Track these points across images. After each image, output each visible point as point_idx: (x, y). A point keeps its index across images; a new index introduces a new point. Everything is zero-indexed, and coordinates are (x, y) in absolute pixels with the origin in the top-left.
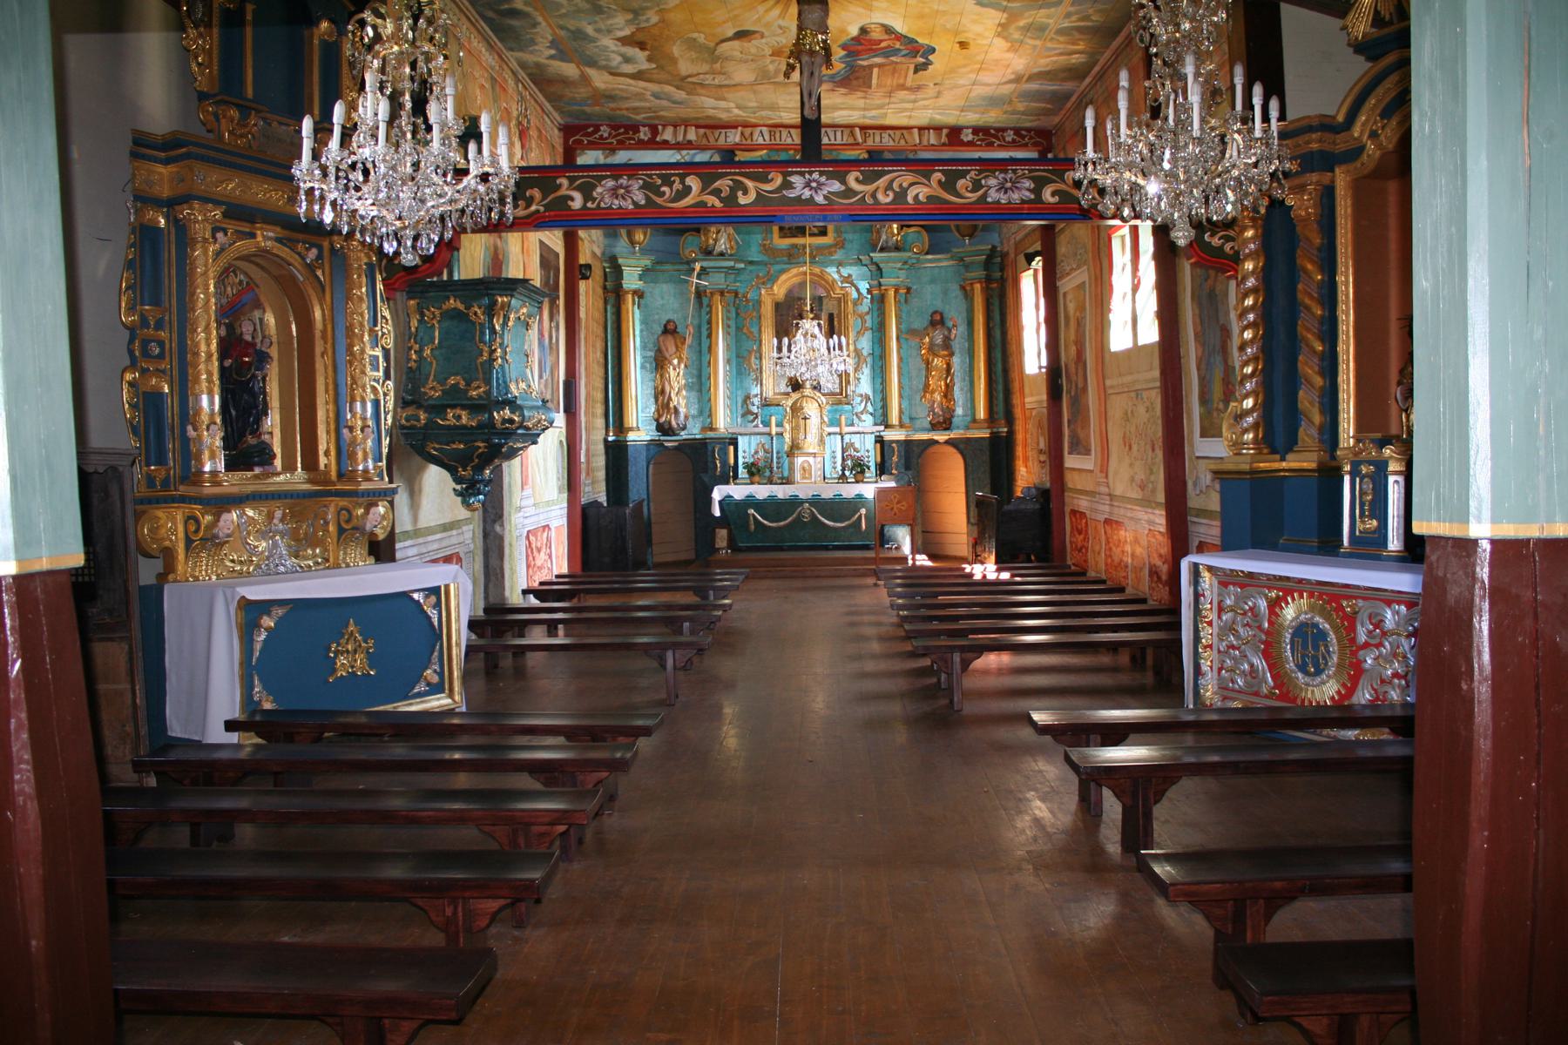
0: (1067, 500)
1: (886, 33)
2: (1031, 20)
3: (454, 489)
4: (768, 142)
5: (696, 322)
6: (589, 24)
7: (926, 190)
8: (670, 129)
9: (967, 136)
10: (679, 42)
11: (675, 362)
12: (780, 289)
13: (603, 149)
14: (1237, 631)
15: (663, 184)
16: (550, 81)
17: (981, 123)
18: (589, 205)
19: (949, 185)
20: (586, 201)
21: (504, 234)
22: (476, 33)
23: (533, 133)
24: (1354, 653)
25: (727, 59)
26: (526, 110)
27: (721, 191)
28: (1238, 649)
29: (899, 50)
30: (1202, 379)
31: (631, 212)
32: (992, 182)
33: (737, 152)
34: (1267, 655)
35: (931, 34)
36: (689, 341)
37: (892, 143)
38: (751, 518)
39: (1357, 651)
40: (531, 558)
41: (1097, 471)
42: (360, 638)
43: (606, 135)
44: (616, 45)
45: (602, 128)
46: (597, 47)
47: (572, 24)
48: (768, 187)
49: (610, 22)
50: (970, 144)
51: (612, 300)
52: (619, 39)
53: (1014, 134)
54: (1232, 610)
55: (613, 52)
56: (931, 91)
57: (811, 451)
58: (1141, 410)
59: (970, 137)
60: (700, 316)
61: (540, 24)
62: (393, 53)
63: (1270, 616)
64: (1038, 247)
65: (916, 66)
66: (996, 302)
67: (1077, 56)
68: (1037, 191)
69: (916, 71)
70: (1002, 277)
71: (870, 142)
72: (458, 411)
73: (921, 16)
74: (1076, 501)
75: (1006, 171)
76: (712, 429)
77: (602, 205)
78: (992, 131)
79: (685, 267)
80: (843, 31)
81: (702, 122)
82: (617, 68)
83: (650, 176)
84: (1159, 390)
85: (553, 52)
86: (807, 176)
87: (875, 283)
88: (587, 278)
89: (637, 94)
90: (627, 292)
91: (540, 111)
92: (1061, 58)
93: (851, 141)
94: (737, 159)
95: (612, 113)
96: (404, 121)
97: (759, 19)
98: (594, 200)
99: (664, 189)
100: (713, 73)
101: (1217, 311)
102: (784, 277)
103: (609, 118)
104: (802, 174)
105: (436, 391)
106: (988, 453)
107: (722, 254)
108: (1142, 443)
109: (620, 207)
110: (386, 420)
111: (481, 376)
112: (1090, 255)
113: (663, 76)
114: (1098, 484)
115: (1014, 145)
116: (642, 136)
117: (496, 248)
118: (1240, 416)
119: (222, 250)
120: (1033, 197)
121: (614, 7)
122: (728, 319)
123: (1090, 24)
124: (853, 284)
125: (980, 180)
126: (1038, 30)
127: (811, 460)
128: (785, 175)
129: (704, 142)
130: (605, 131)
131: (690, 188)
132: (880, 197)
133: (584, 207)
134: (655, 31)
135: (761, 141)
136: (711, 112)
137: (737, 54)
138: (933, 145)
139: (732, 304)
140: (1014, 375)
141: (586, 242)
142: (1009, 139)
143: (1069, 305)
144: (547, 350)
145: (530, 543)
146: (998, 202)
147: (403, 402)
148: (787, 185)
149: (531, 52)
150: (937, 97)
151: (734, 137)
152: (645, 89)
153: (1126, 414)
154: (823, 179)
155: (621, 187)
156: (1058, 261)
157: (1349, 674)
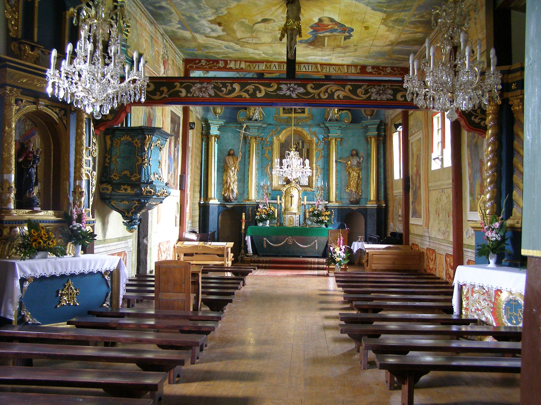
0: (410, 239)
1: (331, 21)
3: (123, 222)
4: (278, 70)
5: (243, 151)
6: (196, 14)
7: (343, 93)
8: (233, 63)
9: (369, 70)
10: (236, 23)
11: (233, 168)
12: (282, 137)
13: (203, 71)
14: (480, 302)
15: (223, 87)
16: (178, 39)
17: (375, 64)
18: (189, 95)
19: (354, 91)
20: (187, 93)
21: (154, 107)
22: (144, 16)
23: (170, 62)
26: (167, 51)
27: (249, 91)
28: (480, 310)
29: (337, 29)
30: (471, 184)
31: (208, 99)
32: (374, 90)
33: (265, 74)
34: (493, 314)
35: (351, 22)
36: (239, 159)
37: (334, 72)
38: (265, 242)
40: (160, 255)
41: (424, 225)
42: (73, 288)
43: (204, 64)
44: (208, 24)
45: (202, 61)
46: (200, 24)
47: (188, 14)
48: (271, 90)
49: (205, 13)
50: (370, 73)
51: (205, 139)
52: (209, 21)
53: (391, 69)
54: (478, 292)
55: (207, 27)
56: (352, 48)
57: (294, 212)
58: (444, 198)
59: (370, 70)
60: (245, 148)
61: (173, 13)
62: (95, 23)
64: (400, 121)
65: (345, 37)
66: (382, 147)
67: (419, 34)
68: (394, 95)
69: (345, 39)
70: (385, 135)
71: (324, 71)
72: (126, 187)
73: (346, 14)
74: (414, 240)
75: (380, 86)
76: (248, 200)
77: (195, 95)
78: (381, 68)
79: (239, 125)
80: (311, 20)
81: (247, 60)
82: (209, 34)
83: (217, 83)
84: (451, 189)
85: (179, 26)
86: (289, 85)
88: (193, 129)
89: (218, 46)
90: (212, 136)
91: (174, 52)
92: (411, 35)
93: (316, 70)
94: (265, 77)
95: (206, 54)
96: (98, 53)
97: (273, 14)
98: (191, 93)
99: (223, 89)
100: (252, 37)
101: (478, 153)
103: (206, 56)
104: (286, 84)
105: (117, 177)
106: (376, 216)
107: (256, 120)
109: (203, 97)
110: (92, 189)
111: (137, 171)
112: (423, 126)
113: (230, 38)
114: (424, 232)
115: (390, 74)
116: (220, 65)
117: (150, 113)
118: (484, 202)
119: (20, 109)
120: (392, 98)
121: (207, 6)
123: (424, 19)
125: (368, 89)
127: (294, 216)
128: (279, 84)
129: (249, 69)
130: (203, 62)
133: (186, 96)
135: (274, 69)
136: (252, 55)
137: (263, 29)
138: (353, 73)
139: (260, 143)
140: (389, 180)
141: (193, 112)
142: (388, 71)
144: (173, 161)
145: (160, 248)
146: (376, 100)
147: (100, 181)
148: (279, 89)
149: (170, 26)
150: (355, 52)
151: (262, 67)
152: (221, 44)
153: (437, 199)
154: (296, 87)
155: (204, 87)
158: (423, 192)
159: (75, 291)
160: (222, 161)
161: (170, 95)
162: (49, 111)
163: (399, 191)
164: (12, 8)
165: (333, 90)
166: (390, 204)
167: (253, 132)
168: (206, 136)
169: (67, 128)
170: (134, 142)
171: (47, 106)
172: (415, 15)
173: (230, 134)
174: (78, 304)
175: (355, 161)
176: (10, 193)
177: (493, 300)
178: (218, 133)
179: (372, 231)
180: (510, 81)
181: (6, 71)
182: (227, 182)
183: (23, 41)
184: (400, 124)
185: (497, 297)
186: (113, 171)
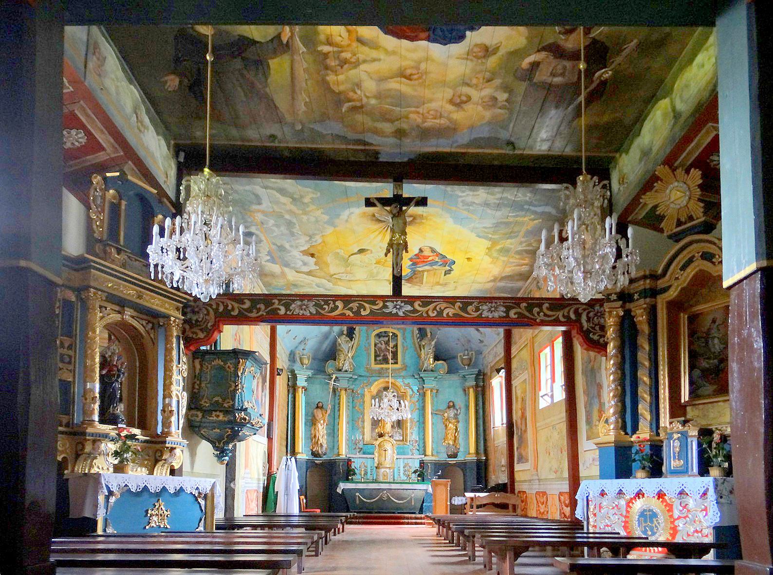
2: (502, 246)
7: (452, 310)
11: (322, 422)
18: (288, 313)
19: (464, 309)
20: (286, 311)
24: (672, 523)
25: (353, 265)
32: (485, 307)
36: (329, 412)
39: (674, 521)
42: (163, 509)
49: (297, 241)
51: (291, 391)
58: (556, 434)
63: (627, 508)
64: (503, 366)
68: (507, 312)
72: (218, 413)
75: (492, 303)
76: (339, 455)
77: (295, 313)
83: (318, 300)
85: (268, 258)
87: (421, 387)
88: (280, 375)
89: (309, 284)
99: (325, 306)
102: (376, 383)
104: (393, 302)
107: (346, 371)
108: (556, 450)
109: (303, 315)
113: (322, 274)
114: (532, 475)
122: (348, 402)
123: (531, 248)
124: (410, 388)
126: (505, 251)
127: (388, 470)
128: (384, 302)
131: (338, 307)
132: (430, 313)
133: (286, 314)
134: (319, 248)
143: (517, 391)
146: (488, 317)
147: (189, 408)
148: (385, 306)
152: (312, 281)
154: (403, 304)
156: (512, 371)
157: (670, 533)
158: (530, 435)
159: (165, 512)
160: (310, 414)
161: (268, 313)
162: (135, 323)
163: (501, 440)
164: (97, 208)
165: (442, 308)
166: (492, 456)
167: (343, 384)
168: (292, 388)
169: (154, 343)
170: (227, 366)
171: (133, 317)
172: (521, 243)
173: (318, 386)
174: (168, 527)
175: (452, 413)
176: (94, 403)
177: (624, 513)
178: (305, 384)
179: (472, 481)
180: (632, 291)
181: (91, 272)
182: (315, 436)
183: (110, 243)
184: (502, 368)
185: (629, 509)
186: (203, 397)
